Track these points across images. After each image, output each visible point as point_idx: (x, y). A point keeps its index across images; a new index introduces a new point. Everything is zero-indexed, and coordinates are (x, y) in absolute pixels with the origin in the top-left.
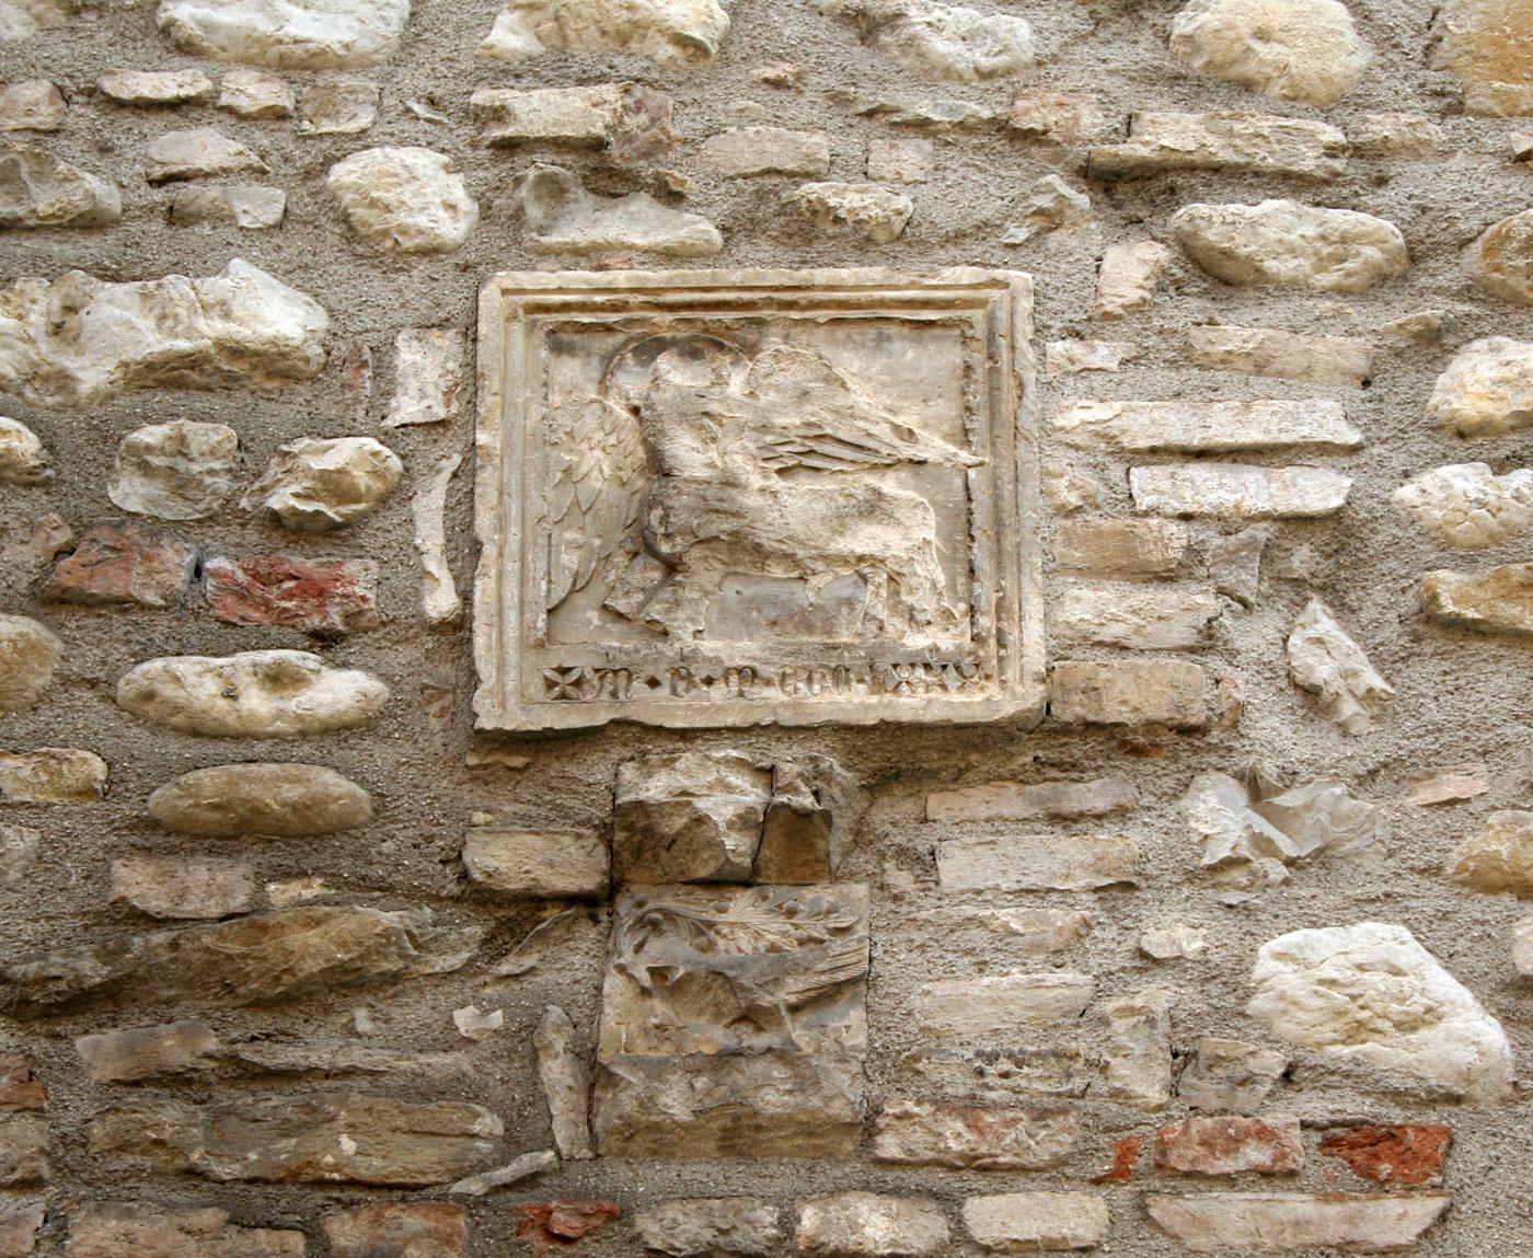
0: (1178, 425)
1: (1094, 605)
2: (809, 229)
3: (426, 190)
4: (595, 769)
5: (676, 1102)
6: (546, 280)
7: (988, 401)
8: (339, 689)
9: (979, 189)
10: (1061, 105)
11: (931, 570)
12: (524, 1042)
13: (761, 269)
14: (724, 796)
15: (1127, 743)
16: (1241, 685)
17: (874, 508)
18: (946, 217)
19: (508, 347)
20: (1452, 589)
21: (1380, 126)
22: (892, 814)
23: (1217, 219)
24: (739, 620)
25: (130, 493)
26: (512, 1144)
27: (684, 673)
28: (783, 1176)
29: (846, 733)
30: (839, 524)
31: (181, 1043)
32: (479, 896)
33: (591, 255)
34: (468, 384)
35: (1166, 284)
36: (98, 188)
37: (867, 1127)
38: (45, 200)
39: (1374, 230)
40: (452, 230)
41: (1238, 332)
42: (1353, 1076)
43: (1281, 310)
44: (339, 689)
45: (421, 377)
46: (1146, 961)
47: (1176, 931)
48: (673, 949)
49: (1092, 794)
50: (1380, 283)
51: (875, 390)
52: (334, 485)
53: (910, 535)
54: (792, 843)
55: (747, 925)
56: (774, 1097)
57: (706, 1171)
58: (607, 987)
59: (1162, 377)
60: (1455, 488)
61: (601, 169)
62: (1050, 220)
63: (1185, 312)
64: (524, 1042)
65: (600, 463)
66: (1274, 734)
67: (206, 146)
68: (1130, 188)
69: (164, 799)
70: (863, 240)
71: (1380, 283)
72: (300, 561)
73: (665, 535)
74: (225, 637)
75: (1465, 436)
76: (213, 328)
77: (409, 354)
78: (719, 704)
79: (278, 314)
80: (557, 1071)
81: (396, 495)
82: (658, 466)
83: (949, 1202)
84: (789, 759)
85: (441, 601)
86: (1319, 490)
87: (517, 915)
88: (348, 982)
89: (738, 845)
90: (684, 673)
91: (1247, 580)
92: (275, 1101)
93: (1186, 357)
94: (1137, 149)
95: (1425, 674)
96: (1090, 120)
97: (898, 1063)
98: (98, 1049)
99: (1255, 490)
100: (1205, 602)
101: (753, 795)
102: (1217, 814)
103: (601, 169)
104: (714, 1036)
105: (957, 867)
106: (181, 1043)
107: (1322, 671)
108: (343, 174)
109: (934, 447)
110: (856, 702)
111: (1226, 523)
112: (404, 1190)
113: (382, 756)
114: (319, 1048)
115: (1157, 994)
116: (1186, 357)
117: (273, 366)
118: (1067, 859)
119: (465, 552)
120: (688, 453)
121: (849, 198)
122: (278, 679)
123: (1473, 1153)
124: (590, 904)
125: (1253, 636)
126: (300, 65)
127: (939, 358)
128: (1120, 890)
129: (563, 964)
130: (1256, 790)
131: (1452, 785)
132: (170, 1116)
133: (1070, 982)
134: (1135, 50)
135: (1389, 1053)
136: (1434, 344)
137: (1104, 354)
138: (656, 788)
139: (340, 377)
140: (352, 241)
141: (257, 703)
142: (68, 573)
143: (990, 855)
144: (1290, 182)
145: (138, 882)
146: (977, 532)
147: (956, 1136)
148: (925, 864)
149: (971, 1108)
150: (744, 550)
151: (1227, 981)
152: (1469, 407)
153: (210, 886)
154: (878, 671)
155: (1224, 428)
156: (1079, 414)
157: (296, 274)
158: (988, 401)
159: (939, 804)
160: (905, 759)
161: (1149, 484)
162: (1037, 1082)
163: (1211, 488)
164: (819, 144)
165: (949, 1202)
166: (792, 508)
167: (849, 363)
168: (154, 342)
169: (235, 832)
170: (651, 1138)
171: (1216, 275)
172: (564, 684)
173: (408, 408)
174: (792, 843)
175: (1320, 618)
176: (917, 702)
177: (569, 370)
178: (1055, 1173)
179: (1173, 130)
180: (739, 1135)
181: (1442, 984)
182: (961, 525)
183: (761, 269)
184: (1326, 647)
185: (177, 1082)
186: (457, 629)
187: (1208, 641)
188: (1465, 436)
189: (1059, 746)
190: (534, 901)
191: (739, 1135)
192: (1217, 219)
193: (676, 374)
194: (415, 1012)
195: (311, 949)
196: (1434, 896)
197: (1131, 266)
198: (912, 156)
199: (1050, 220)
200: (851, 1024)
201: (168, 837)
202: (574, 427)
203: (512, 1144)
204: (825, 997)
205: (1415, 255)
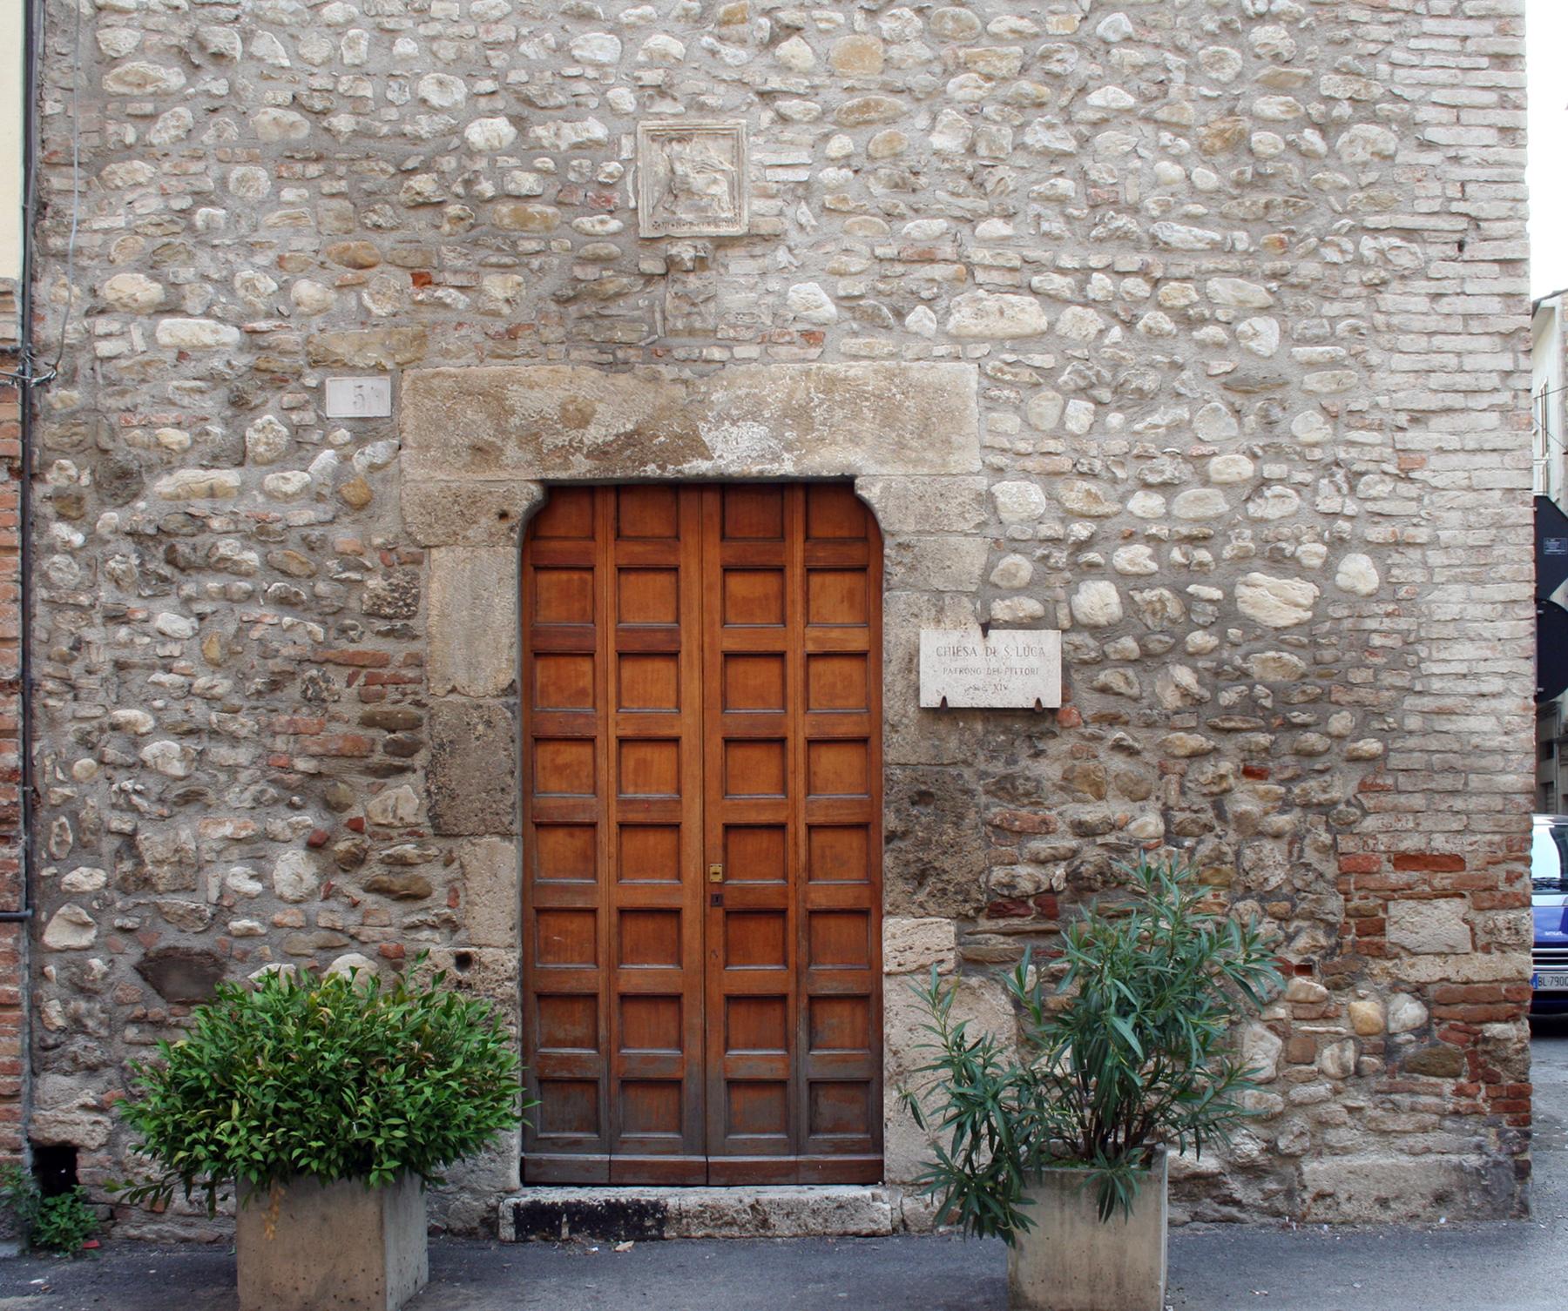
0: (775, 159)
1: (759, 205)
2: (702, 107)
3: (624, 98)
4: (662, 245)
5: (680, 325)
6: (654, 124)
7: (738, 156)
8: (614, 225)
9: (737, 97)
10: (215, 110)
11: (726, 198)
12: (651, 308)
13: (693, 120)
14: (686, 253)
15: (765, 239)
16: (788, 225)
17: (715, 181)
18: (729, 105)
19: (644, 141)
20: (828, 199)
21: (817, 81)
22: (720, 254)
23: (785, 105)
24: (688, 210)
25: (572, 176)
26: (651, 333)
27: (680, 223)
28: (700, 341)
29: (711, 238)
30: (708, 185)
31: (589, 308)
32: (642, 274)
33: (658, 115)
34: (635, 150)
35: (773, 122)
36: (561, 99)
37: (715, 331)
38: (552, 102)
39: (815, 106)
40: (631, 108)
41: (788, 135)
42: (807, 320)
43: (797, 128)
44: (614, 225)
45: (627, 142)
46: (768, 292)
47: (774, 284)
48: (678, 287)
49: (758, 250)
50: (817, 120)
51: (716, 153)
52: (610, 175)
53: (721, 189)
54: (701, 263)
55: (693, 282)
56: (698, 325)
57: (685, 340)
58: (665, 293)
59: (774, 147)
60: (830, 174)
61: (661, 91)
62: (750, 105)
63: (776, 129)
64: (651, 308)
65: (662, 170)
66: (794, 237)
67: (582, 87)
68: (767, 96)
69: (582, 252)
70: (714, 111)
71: (817, 120)
72: (606, 193)
73: (675, 189)
74: (592, 212)
75: (832, 161)
76: (586, 135)
77: (624, 141)
78: (684, 231)
79: (598, 131)
80: (658, 316)
81: (622, 176)
82: (673, 171)
83: (730, 348)
84: (699, 244)
85: (632, 204)
86: (803, 175)
87: (649, 278)
88: (618, 295)
89: (690, 265)
90: (680, 223)
91: (789, 197)
92: (606, 322)
93: (778, 141)
94: (767, 88)
95: (824, 219)
96: (758, 80)
97: (721, 316)
98: (573, 310)
99: (783, 175)
100: (780, 203)
101: (692, 253)
102: (782, 256)
103: (661, 91)
104: (686, 308)
105: (732, 268)
106: (589, 308)
107: (803, 221)
108: (610, 94)
109: (727, 166)
110: (711, 230)
111: (785, 183)
112: (630, 345)
113: (622, 240)
114: (613, 310)
115: (770, 299)
116: (778, 141)
117: (598, 143)
118: (752, 266)
119: (636, 193)
120: (680, 169)
121: (710, 100)
122: (602, 222)
123: (829, 337)
124: (664, 276)
125: (790, 211)
126: (599, 66)
127: (726, 144)
128: (763, 274)
129: (659, 289)
130: (790, 250)
131: (828, 248)
132: (587, 327)
133: (753, 296)
134: (768, 60)
135: (813, 314)
136: (826, 137)
137: (761, 140)
138: (674, 251)
139: (608, 147)
140: (609, 111)
141: (598, 228)
142: (561, 197)
143: (739, 265)
144: (799, 95)
145: (579, 272)
146: (736, 188)
147: (732, 333)
148: (726, 267)
149: (734, 326)
150: (690, 192)
151: (782, 295)
152: (833, 154)
153: (591, 272)
154: (716, 222)
155: (785, 160)
156: (756, 156)
157: (601, 119)
158: (738, 156)
159: (730, 252)
160: (722, 243)
161: (769, 174)
162: (747, 320)
163: (783, 175)
164: (703, 86)
165: (730, 348)
166: (698, 181)
167: (710, 144)
168: (576, 139)
169: (596, 260)
170: (675, 333)
171: (783, 119)
172: (656, 226)
173: (625, 155)
174: (701, 263)
175: (804, 207)
176: (724, 230)
177: (656, 146)
178: (750, 341)
179: (775, 83)
180: (692, 332)
181: (824, 297)
182: (732, 185)
183: (693, 120)
184: (804, 213)
185: (588, 318)
186: (636, 209)
187: (781, 213)
188: (832, 161)
189: (756, 239)
190: (652, 275)
191: (692, 332)
192: (785, 105)
193: (676, 146)
194: (631, 301)
195: (611, 288)
196: (823, 276)
197: (767, 116)
198: (722, 88)
199: (750, 105)
200: (712, 305)
201: (585, 261)
202: (657, 158)
203: (651, 333)
204: (707, 300)
205: (824, 113)
